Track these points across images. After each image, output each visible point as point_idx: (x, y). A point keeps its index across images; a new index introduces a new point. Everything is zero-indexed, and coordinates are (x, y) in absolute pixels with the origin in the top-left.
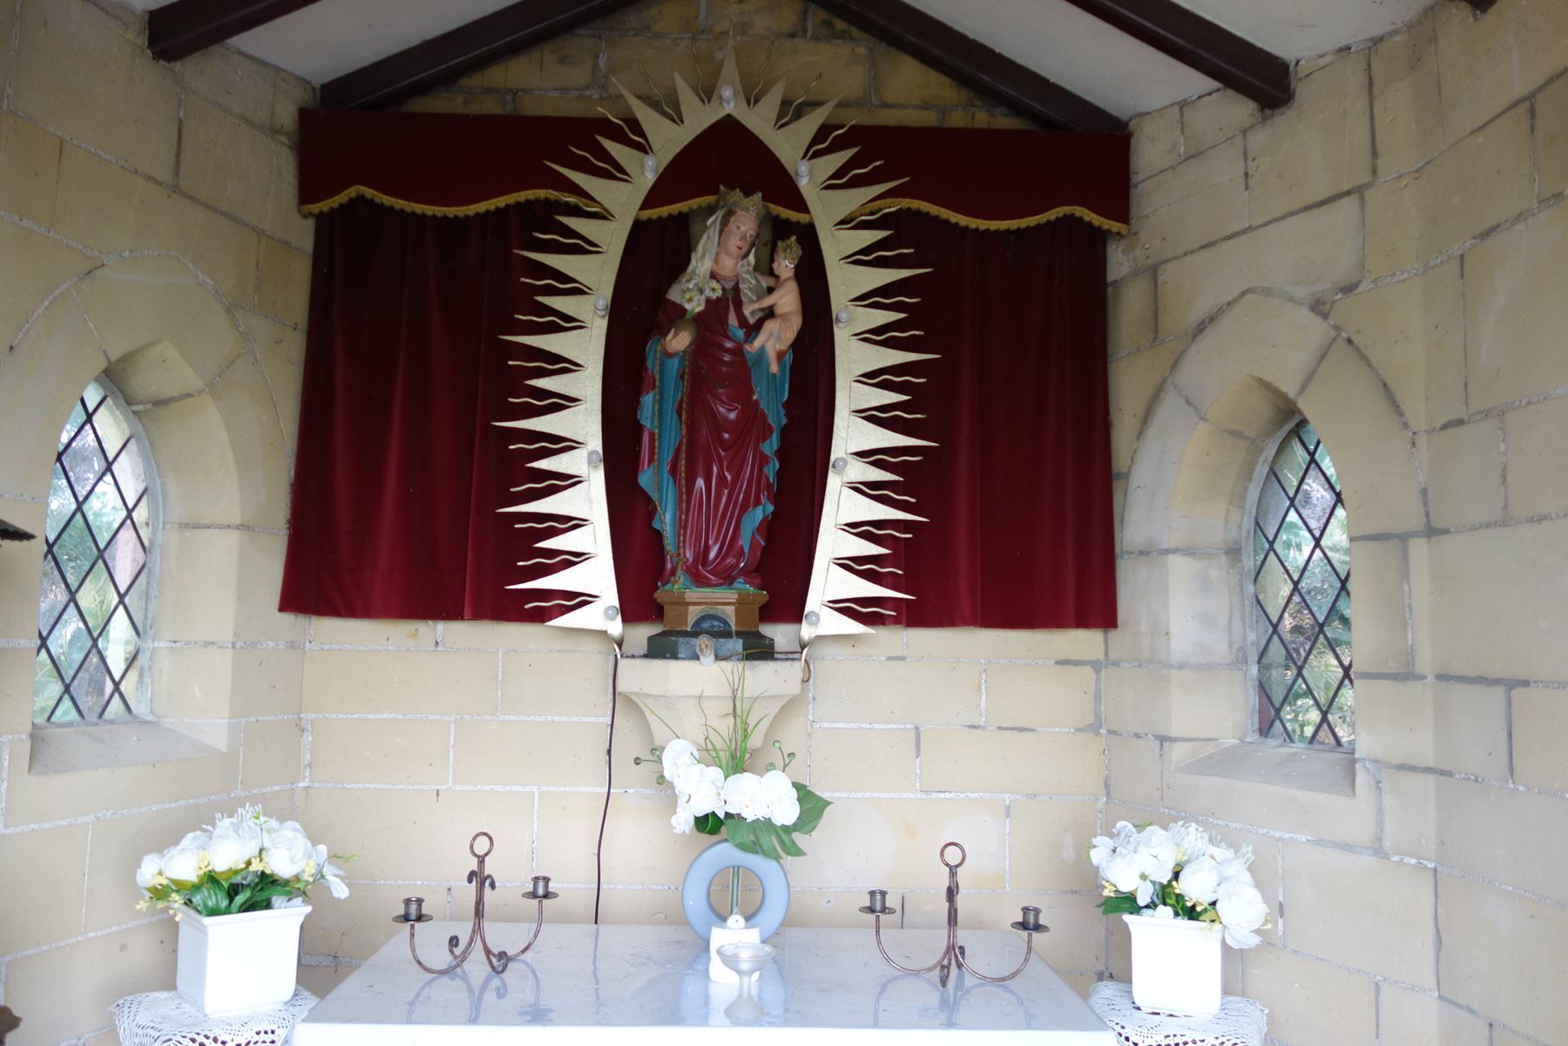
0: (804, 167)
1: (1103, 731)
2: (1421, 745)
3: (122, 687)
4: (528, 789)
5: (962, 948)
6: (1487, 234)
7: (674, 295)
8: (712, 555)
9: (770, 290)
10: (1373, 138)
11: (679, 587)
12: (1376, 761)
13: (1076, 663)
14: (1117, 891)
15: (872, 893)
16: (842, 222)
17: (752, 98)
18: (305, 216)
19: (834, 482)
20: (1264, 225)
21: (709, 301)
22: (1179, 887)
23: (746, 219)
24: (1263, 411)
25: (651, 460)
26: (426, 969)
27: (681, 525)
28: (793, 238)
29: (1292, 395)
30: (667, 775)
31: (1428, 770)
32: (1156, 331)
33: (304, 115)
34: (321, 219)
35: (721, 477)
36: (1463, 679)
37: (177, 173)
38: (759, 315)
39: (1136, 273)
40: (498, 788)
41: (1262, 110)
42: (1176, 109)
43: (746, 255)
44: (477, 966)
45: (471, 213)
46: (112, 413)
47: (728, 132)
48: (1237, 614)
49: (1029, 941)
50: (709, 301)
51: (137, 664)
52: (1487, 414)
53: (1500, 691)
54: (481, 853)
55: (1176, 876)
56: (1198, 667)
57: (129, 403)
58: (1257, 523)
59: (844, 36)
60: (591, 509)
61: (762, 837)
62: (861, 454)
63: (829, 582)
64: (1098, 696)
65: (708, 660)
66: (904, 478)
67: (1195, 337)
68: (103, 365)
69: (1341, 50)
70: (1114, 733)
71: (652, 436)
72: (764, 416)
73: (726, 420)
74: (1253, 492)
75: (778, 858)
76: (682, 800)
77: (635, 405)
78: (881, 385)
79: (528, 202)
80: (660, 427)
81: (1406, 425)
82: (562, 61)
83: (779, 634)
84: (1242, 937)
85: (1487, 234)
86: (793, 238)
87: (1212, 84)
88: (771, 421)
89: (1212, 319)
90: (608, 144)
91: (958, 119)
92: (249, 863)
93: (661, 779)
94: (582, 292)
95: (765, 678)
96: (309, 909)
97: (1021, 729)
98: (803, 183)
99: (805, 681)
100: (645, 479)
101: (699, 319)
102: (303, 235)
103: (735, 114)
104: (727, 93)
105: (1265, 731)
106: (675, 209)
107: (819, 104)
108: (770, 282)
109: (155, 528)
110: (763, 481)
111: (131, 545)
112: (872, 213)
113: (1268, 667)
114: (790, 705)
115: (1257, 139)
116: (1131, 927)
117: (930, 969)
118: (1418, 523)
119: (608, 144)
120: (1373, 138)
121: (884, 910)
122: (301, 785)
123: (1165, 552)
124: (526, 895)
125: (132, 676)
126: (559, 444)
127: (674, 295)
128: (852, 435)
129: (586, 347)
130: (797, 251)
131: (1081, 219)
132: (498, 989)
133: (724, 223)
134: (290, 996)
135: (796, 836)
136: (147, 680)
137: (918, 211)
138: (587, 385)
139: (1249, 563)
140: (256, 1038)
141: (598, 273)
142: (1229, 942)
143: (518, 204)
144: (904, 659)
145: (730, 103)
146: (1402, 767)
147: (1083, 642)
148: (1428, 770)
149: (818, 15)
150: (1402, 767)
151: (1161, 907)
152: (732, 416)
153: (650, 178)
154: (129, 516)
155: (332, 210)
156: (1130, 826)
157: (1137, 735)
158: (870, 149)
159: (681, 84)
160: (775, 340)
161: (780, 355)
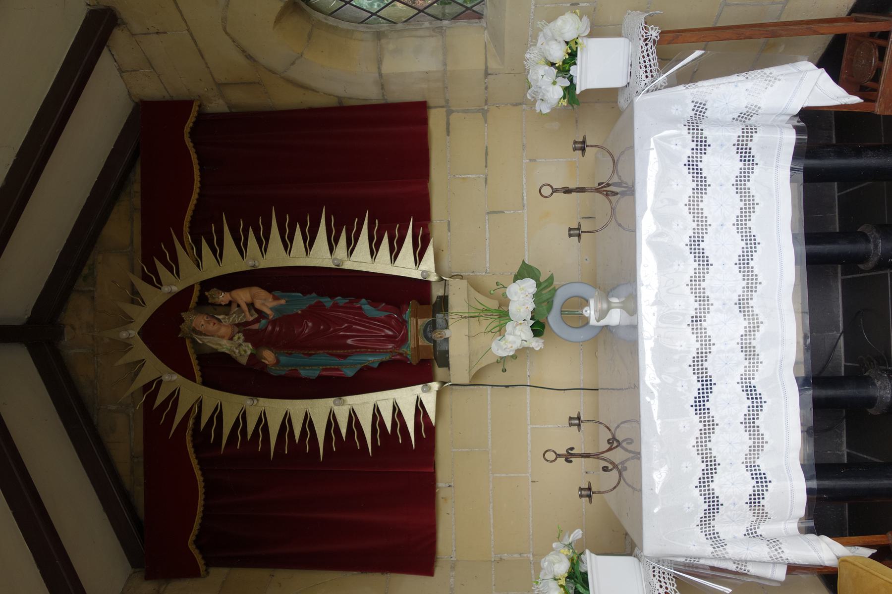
0: (166, 289)
1: (486, 108)
4: (529, 431)
5: (599, 184)
7: (244, 361)
8: (390, 333)
9: (239, 306)
11: (408, 350)
13: (448, 124)
14: (564, 97)
15: (570, 236)
16: (198, 266)
17: (128, 320)
18: (208, 573)
19: (348, 265)
20: (186, 22)
21: (246, 341)
22: (559, 63)
23: (197, 321)
25: (338, 370)
26: (618, 484)
27: (374, 351)
28: (207, 293)
30: (511, 354)
32: (254, 83)
33: (148, 577)
34: (208, 564)
38: (253, 312)
40: (529, 448)
41: (119, 25)
42: (123, 74)
43: (219, 320)
44: (617, 456)
45: (202, 478)
47: (148, 333)
49: (592, 146)
50: (246, 341)
54: (554, 456)
55: (553, 64)
58: (362, 22)
60: (367, 403)
61: (544, 298)
62: (331, 250)
63: (405, 266)
64: (466, 111)
65: (447, 333)
66: (344, 226)
67: (255, 61)
70: (486, 102)
71: (324, 370)
72: (310, 306)
74: (345, 25)
75: (555, 290)
76: (525, 344)
77: (307, 380)
78: (291, 241)
79: (194, 446)
80: (318, 365)
83: (437, 292)
84: (584, 26)
86: (207, 293)
87: (105, 52)
88: (313, 303)
89: (244, 51)
90: (158, 402)
91: (137, 201)
92: (561, 586)
93: (514, 357)
94: (244, 413)
95: (457, 303)
96: (587, 551)
97: (487, 154)
98: (175, 289)
99: (462, 277)
100: (349, 372)
101: (256, 345)
102: (218, 574)
103: (138, 330)
104: (124, 335)
105: (479, 16)
108: (234, 306)
113: (444, 14)
114: (475, 286)
116: (583, 89)
117: (610, 202)
119: (158, 402)
121: (579, 229)
122: (531, 558)
123: (381, 75)
124: (579, 430)
126: (332, 422)
127: (244, 361)
128: (321, 256)
130: (214, 291)
131: (192, 128)
132: (628, 443)
134: (636, 559)
135: (542, 280)
137: (191, 222)
138: (297, 408)
139: (385, 27)
140: (657, 577)
141: (233, 405)
142: (586, 34)
143: (195, 452)
144: (449, 222)
145: (132, 333)
147: (436, 121)
151: (571, 73)
152: (310, 324)
153: (176, 377)
155: (203, 558)
156: (530, 91)
157: (486, 88)
158: (155, 251)
159: (121, 362)
160: (266, 302)
161: (276, 298)
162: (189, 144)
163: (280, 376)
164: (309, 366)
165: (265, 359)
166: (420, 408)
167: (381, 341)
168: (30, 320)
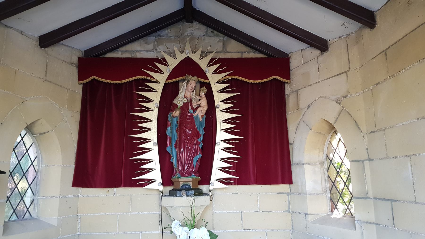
1: (291, 212)
2: (371, 217)
3: (29, 210)
6: (377, 84)
7: (175, 102)
8: (186, 168)
9: (200, 100)
10: (349, 59)
12: (360, 221)
13: (282, 193)
16: (217, 82)
19: (217, 148)
23: (193, 82)
24: (326, 127)
27: (178, 161)
29: (333, 124)
30: (173, 231)
31: (374, 223)
34: (84, 84)
35: (188, 148)
36: (380, 199)
37: (46, 76)
38: (197, 106)
39: (292, 92)
42: (301, 51)
43: (193, 91)
46: (28, 136)
47: (188, 60)
48: (323, 180)
50: (184, 103)
51: (33, 203)
52: (381, 130)
53: (389, 202)
56: (314, 194)
57: (33, 134)
58: (330, 142)
59: (216, 36)
62: (224, 141)
63: (216, 174)
66: (236, 146)
68: (26, 126)
69: (340, 37)
70: (294, 212)
72: (199, 132)
73: (188, 133)
74: (325, 148)
77: (165, 130)
80: (172, 136)
81: (361, 132)
82: (146, 43)
83: (204, 188)
85: (377, 84)
88: (200, 133)
90: (158, 64)
97: (269, 212)
100: (168, 149)
101: (182, 107)
102: (79, 89)
106: (175, 80)
107: (212, 52)
108: (200, 98)
109: (39, 167)
110: (199, 148)
111: (33, 171)
112: (225, 80)
113: (333, 194)
115: (321, 59)
118: (366, 157)
119: (158, 64)
120: (349, 59)
122: (77, 234)
123: (304, 164)
125: (32, 206)
127: (175, 102)
128: (221, 136)
129: (153, 115)
131: (278, 79)
133: (187, 84)
136: (36, 207)
138: (153, 125)
139: (326, 167)
141: (156, 97)
146: (367, 222)
148: (374, 223)
149: (210, 30)
150: (367, 222)
152: (190, 132)
154: (32, 164)
158: (223, 64)
159: (175, 49)
160: (200, 113)
162: (270, 78)
163: (167, 118)
164: (172, 131)
165: (175, 112)
166: (151, 181)
167: (182, 164)
168: (194, 9)
